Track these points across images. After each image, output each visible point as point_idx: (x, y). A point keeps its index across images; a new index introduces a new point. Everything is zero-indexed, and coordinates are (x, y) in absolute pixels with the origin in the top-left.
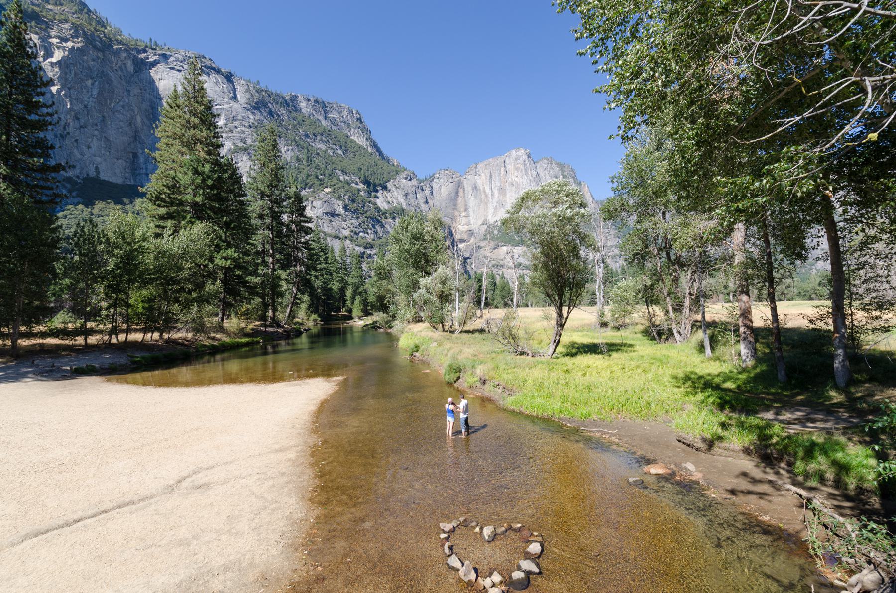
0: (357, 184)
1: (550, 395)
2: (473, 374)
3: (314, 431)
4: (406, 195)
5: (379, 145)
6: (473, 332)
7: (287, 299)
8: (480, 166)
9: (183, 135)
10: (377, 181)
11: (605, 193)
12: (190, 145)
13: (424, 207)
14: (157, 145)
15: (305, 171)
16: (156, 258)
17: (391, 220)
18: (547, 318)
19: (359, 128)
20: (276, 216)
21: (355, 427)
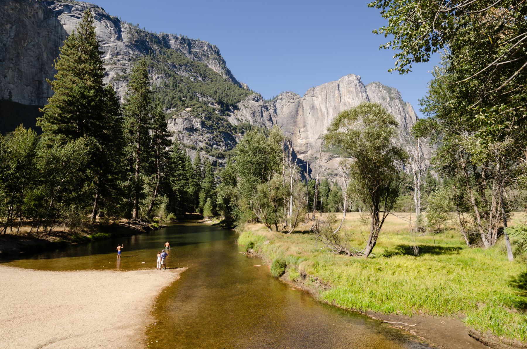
0: (213, 104)
1: (362, 290)
2: (296, 269)
3: (153, 313)
4: (254, 113)
5: (233, 73)
6: (304, 232)
7: (148, 200)
8: (317, 89)
9: (76, 68)
10: (229, 102)
11: (415, 112)
12: (79, 74)
13: (268, 124)
14: (55, 76)
15: (171, 94)
16: (48, 163)
17: (239, 134)
18: (365, 223)
19: (217, 59)
20: (144, 131)
21: (187, 311)
